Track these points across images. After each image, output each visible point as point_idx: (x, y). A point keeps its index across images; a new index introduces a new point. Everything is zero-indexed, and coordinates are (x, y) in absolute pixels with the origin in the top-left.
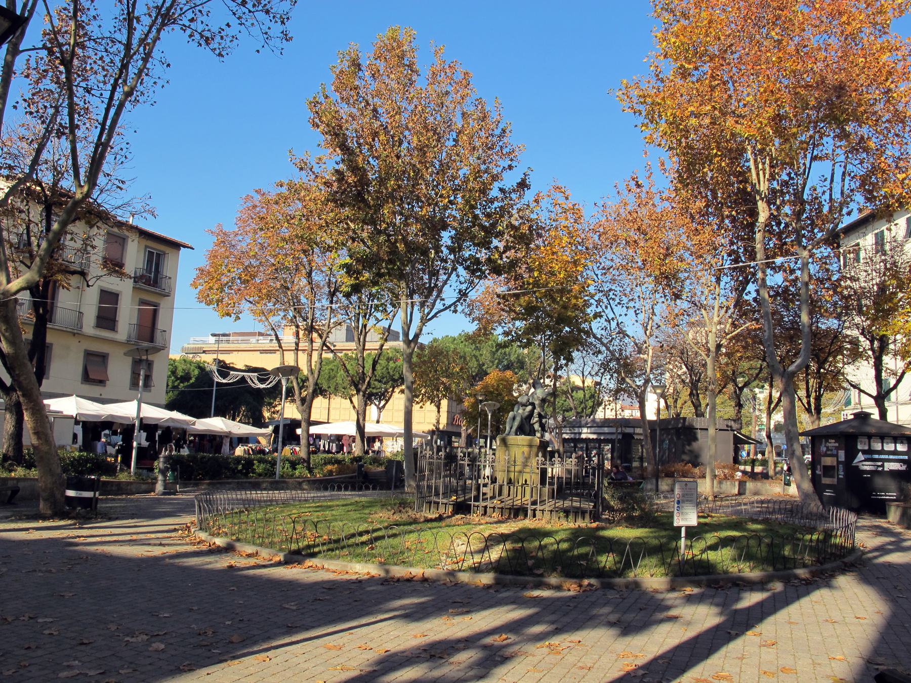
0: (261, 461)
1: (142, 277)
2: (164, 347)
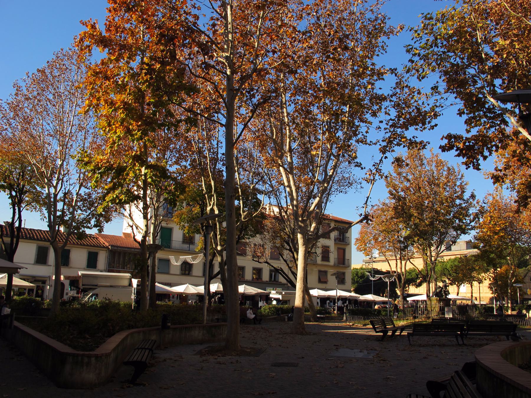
1: (337, 239)
2: (349, 266)
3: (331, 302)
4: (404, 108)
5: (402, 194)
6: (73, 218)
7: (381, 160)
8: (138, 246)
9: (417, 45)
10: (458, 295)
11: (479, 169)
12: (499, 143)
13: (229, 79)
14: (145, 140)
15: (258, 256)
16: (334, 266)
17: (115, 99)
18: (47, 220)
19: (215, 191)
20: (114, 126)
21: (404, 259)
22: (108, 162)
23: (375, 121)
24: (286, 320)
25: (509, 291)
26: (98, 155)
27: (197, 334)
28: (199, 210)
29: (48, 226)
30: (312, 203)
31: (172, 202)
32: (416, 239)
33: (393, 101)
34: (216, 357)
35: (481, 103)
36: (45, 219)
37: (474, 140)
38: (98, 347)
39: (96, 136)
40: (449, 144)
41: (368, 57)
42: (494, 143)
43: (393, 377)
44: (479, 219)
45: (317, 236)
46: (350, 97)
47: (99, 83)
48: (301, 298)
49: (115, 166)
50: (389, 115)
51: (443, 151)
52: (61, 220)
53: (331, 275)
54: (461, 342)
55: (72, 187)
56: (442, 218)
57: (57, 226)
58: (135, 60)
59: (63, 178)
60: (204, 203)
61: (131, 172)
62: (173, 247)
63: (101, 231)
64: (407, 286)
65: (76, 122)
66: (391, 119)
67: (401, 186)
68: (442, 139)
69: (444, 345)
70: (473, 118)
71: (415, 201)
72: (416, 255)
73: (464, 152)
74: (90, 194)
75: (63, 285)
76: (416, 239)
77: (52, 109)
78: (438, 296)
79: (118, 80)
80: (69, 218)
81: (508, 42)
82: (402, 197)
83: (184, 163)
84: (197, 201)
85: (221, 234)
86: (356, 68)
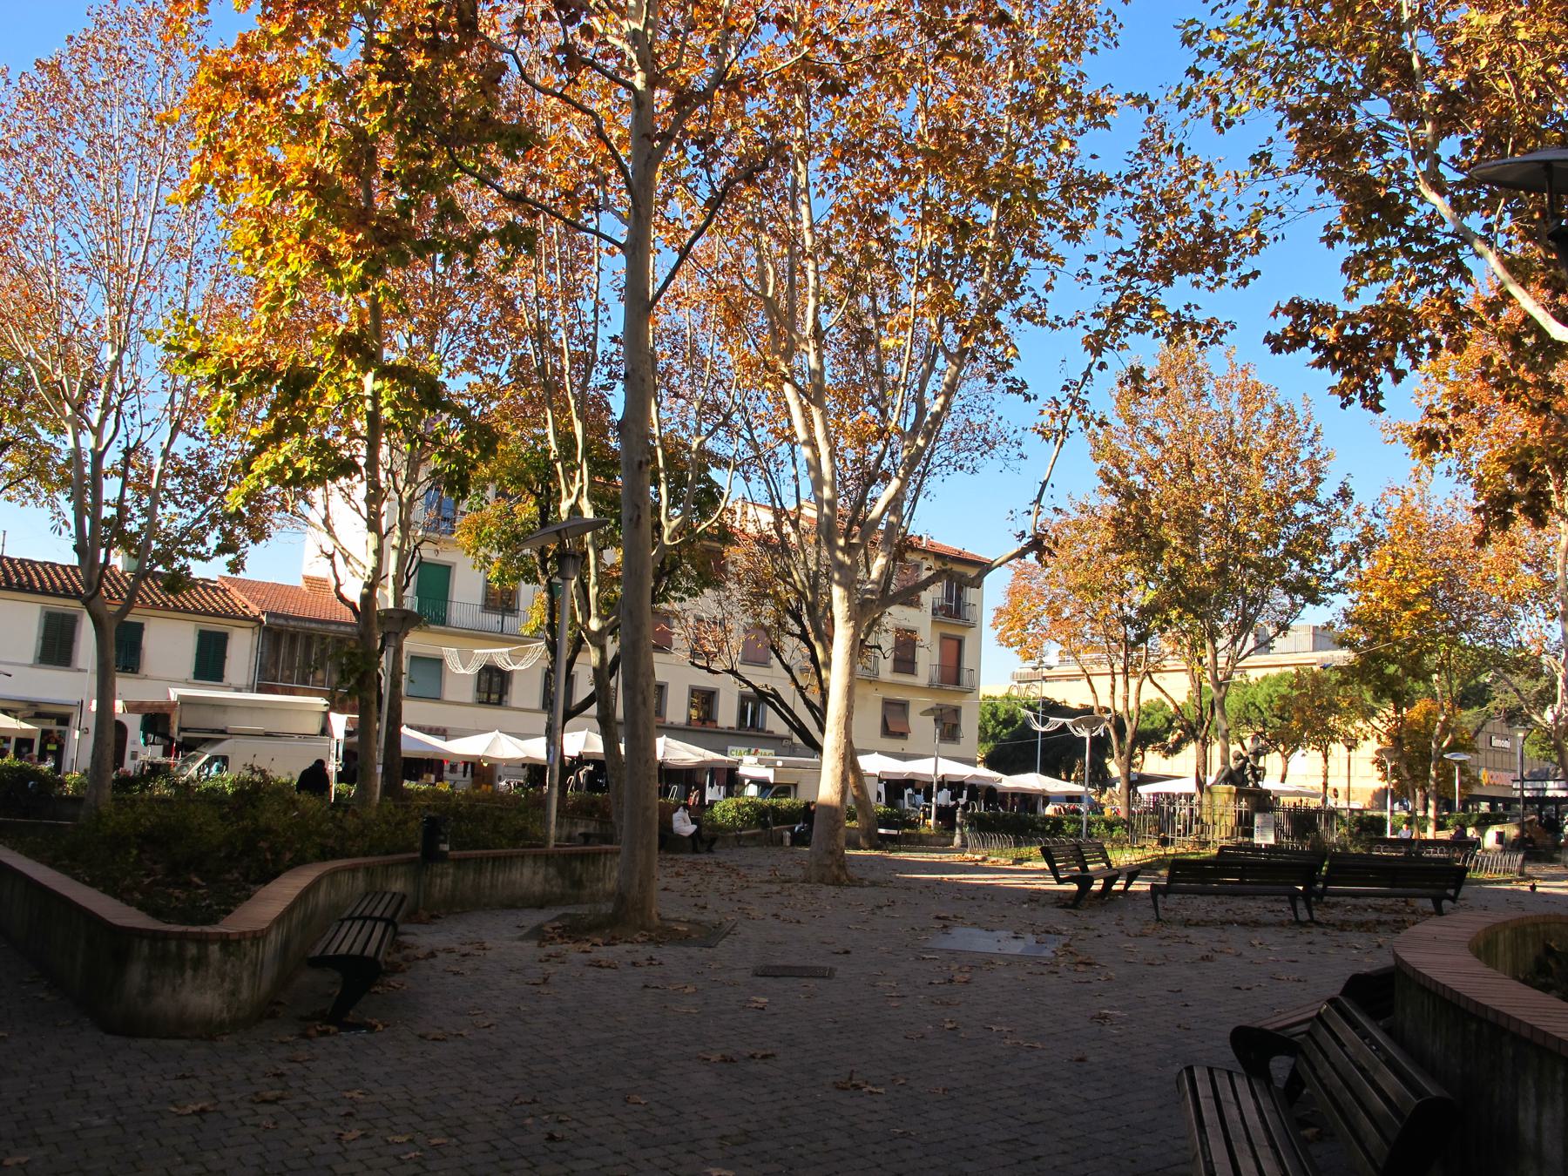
0: (1072, 821)
1: (941, 608)
2: (973, 690)
3: (918, 792)
4: (1162, 218)
5: (1139, 480)
6: (151, 528)
7: (1087, 374)
8: (348, 615)
9: (1211, 22)
10: (1283, 780)
11: (1378, 409)
12: (1444, 332)
13: (641, 103)
14: (375, 290)
15: (707, 654)
16: (930, 688)
17: (281, 160)
18: (73, 531)
19: (586, 451)
20: (279, 245)
21: (1136, 674)
22: (259, 354)
23: (1074, 255)
24: (787, 842)
25: (1433, 773)
26: (231, 332)
27: (528, 876)
28: (537, 509)
29: (76, 548)
30: (874, 500)
31: (457, 483)
32: (1174, 614)
33: (1131, 195)
34: (587, 946)
35: (1393, 212)
36: (64, 528)
37: (1370, 320)
38: (228, 912)
39: (223, 277)
40: (1294, 330)
41: (1063, 54)
42: (1425, 334)
43: (1117, 1013)
44: (1358, 561)
45: (885, 597)
46: (1005, 176)
47: (232, 108)
48: (839, 778)
49: (282, 367)
50: (1119, 235)
51: (1276, 350)
52: (116, 532)
53: (922, 714)
54: (1304, 915)
55: (148, 432)
56: (1253, 556)
57: (103, 551)
58: (346, 41)
59: (120, 403)
60: (549, 489)
61: (332, 388)
62: (453, 623)
63: (235, 567)
64: (1137, 750)
65: (161, 232)
66: (1122, 252)
67: (1137, 457)
68: (1274, 314)
69: (1256, 924)
70: (1369, 255)
71: (1175, 502)
72: (1169, 663)
73: (1337, 355)
74: (205, 455)
75: (121, 729)
76: (1174, 614)
77: (85, 190)
78: (1233, 783)
79: (291, 102)
80: (141, 526)
81: (1496, 19)
82: (1138, 491)
83: (492, 369)
84: (528, 484)
85: (599, 583)
86: (1023, 87)
